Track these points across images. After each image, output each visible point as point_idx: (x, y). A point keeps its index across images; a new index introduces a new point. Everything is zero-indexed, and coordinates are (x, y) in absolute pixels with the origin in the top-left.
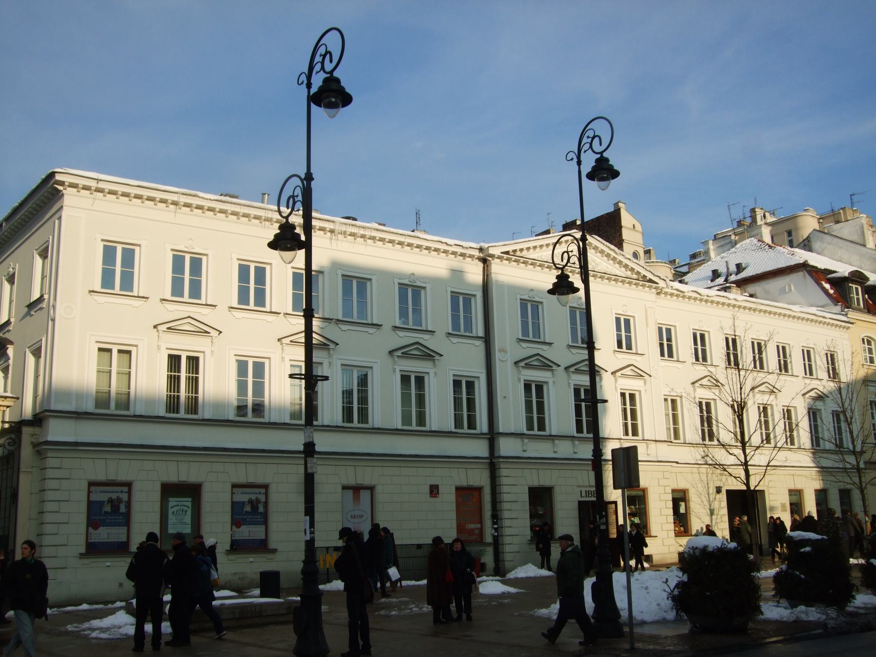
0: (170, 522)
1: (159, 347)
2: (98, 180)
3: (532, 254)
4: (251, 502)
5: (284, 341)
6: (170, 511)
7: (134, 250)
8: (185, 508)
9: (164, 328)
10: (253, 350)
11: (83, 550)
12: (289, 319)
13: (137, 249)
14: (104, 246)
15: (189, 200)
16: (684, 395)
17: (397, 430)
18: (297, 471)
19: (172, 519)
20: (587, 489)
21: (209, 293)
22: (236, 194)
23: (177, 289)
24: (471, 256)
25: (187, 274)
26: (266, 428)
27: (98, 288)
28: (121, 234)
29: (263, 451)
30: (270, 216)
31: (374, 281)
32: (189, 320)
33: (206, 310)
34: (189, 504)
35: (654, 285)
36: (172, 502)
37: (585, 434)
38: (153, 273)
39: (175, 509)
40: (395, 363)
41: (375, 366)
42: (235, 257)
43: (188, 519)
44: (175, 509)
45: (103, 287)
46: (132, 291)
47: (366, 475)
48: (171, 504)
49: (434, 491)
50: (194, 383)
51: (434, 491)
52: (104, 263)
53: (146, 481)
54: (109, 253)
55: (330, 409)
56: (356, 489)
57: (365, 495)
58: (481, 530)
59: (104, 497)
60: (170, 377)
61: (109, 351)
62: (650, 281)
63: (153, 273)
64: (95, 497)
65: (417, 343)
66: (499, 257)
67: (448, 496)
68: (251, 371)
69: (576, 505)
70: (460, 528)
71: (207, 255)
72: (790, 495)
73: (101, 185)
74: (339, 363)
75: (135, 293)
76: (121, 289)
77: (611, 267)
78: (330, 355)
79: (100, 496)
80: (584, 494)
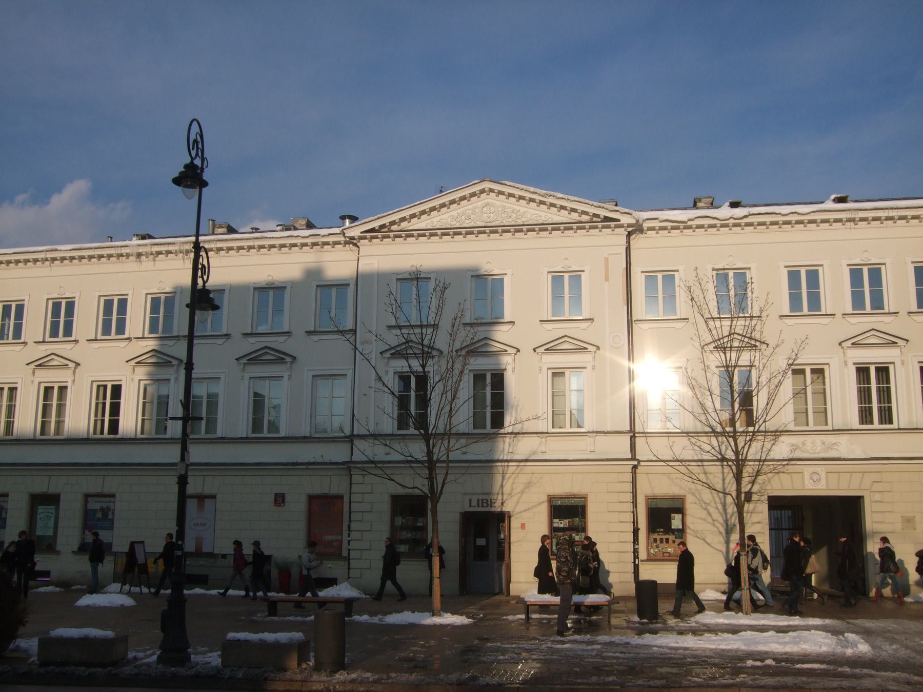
1: (846, 363)
3: (416, 224)
4: (102, 509)
5: (844, 345)
6: (39, 516)
7: (817, 271)
9: (849, 343)
10: (110, 376)
11: (75, 549)
13: (820, 269)
14: (915, 267)
15: (53, 255)
16: (791, 361)
19: (39, 523)
20: (481, 497)
21: (890, 301)
24: (336, 243)
25: (867, 285)
26: (261, 443)
27: (850, 311)
30: (891, 214)
31: (825, 266)
32: (53, 357)
33: (888, 319)
35: (612, 224)
36: (41, 509)
37: (412, 431)
38: (836, 291)
39: (42, 515)
42: (782, 264)
43: (51, 523)
44: (42, 515)
45: (854, 308)
46: (820, 310)
48: (39, 511)
49: (280, 499)
51: (280, 499)
52: (853, 286)
53: (72, 493)
54: (794, 277)
60: (860, 391)
61: (802, 372)
62: (607, 219)
63: (836, 291)
65: (266, 347)
66: (361, 238)
67: (297, 507)
69: (457, 517)
71: (884, 264)
72: (771, 508)
75: (823, 312)
76: (872, 308)
79: (94, 505)
80: (474, 503)
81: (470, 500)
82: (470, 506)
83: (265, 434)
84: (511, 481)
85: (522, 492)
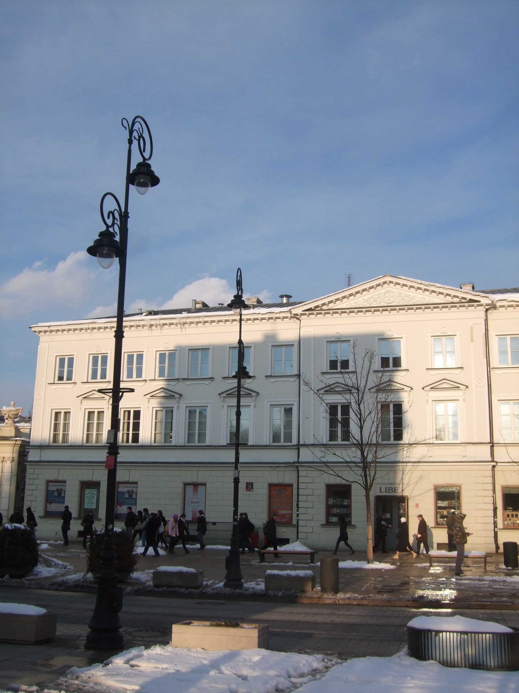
0: (86, 502)
2: (49, 326)
3: (339, 305)
6: (86, 496)
8: (93, 495)
12: (186, 382)
17: (269, 446)
18: (230, 474)
19: (86, 501)
20: (388, 486)
22: (301, 301)
23: (94, 376)
28: (65, 351)
29: (211, 463)
30: (138, 324)
34: (96, 493)
36: (87, 491)
39: (88, 495)
40: (223, 401)
41: (209, 405)
47: (200, 476)
48: (86, 492)
50: (66, 426)
55: (179, 436)
56: (196, 485)
57: (201, 489)
58: (291, 515)
59: (55, 488)
64: (51, 488)
68: (61, 418)
70: (271, 513)
73: (51, 328)
74: (184, 406)
77: (427, 298)
78: (255, 401)
81: (380, 488)
82: (381, 492)
83: (282, 443)
84: (408, 475)
85: (416, 483)
